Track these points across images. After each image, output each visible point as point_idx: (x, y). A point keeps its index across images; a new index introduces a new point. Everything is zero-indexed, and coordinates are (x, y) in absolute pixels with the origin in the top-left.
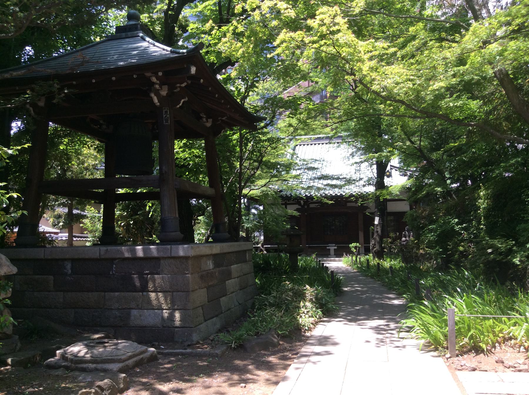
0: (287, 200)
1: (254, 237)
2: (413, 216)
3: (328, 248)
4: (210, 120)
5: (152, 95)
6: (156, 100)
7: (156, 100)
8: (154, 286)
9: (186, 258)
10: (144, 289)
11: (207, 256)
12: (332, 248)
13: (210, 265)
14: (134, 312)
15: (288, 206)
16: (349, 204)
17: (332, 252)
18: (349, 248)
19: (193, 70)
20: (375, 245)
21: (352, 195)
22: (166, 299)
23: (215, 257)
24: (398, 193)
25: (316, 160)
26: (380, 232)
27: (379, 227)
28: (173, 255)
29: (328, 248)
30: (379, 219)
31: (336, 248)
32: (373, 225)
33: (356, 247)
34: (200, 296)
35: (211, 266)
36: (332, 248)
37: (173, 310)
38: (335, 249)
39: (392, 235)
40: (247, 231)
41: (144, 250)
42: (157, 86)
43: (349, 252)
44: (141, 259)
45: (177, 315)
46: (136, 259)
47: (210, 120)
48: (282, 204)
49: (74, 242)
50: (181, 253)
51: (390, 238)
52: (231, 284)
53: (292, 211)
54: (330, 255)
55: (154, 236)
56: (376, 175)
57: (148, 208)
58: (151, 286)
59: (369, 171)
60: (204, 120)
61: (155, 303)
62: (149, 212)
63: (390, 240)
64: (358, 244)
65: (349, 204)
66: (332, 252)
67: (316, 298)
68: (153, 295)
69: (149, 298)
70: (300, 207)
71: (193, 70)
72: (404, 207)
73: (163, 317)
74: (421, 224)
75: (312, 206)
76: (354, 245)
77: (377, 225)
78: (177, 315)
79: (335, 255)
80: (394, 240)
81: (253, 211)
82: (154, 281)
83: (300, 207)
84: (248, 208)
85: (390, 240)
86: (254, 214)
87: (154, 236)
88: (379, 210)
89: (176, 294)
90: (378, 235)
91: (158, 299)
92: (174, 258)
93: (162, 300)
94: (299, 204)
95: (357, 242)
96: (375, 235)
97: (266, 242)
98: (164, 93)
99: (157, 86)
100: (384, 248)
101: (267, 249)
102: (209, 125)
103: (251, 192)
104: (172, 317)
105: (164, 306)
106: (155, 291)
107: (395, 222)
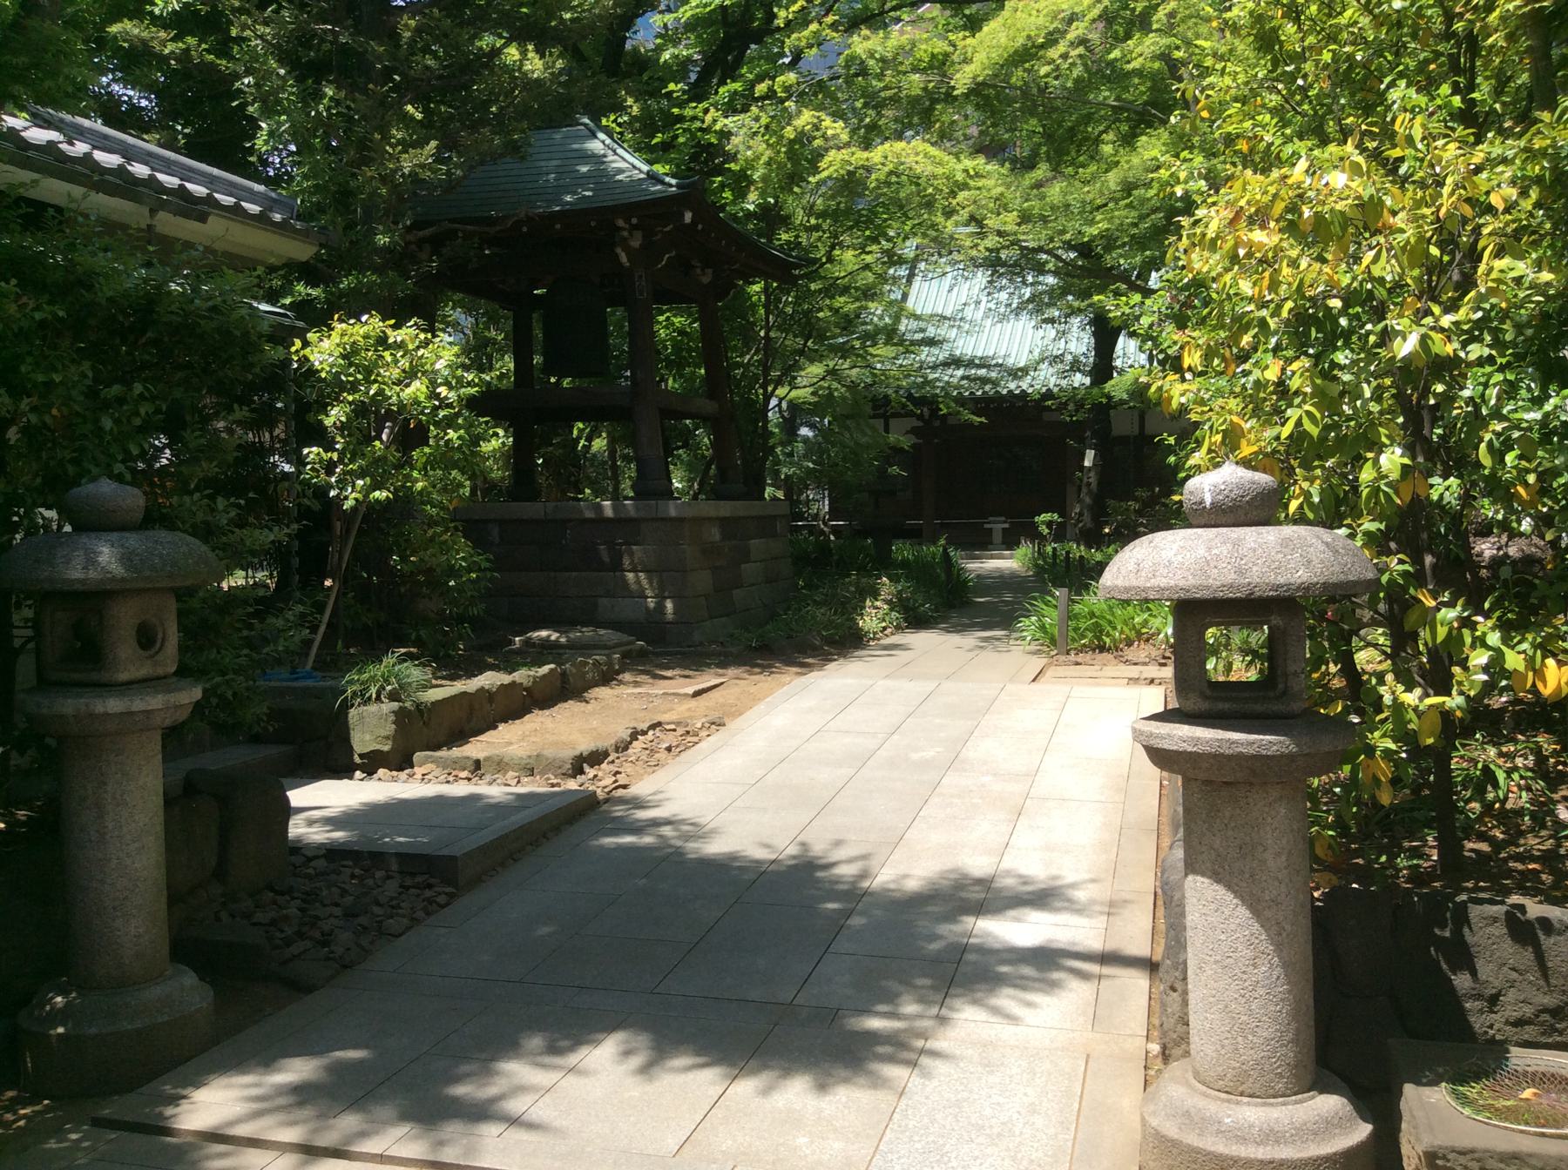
0: (877, 405)
1: (808, 500)
4: (710, 271)
5: (619, 250)
6: (624, 258)
7: (624, 258)
8: (632, 562)
9: (680, 520)
10: (617, 567)
11: (710, 519)
12: (998, 526)
13: (715, 534)
14: (604, 601)
15: (893, 422)
17: (997, 537)
18: (1035, 526)
19: (688, 217)
20: (1081, 514)
22: (651, 583)
23: (723, 522)
24: (1125, 396)
25: (945, 318)
26: (1094, 486)
27: (1092, 474)
28: (660, 515)
32: (1082, 468)
33: (1049, 524)
34: (702, 580)
35: (717, 537)
37: (661, 598)
40: (789, 485)
41: (614, 508)
42: (625, 234)
43: (1033, 534)
44: (609, 520)
45: (669, 605)
46: (601, 521)
47: (710, 271)
48: (874, 417)
50: (673, 513)
51: (1136, 499)
52: (750, 570)
53: (900, 437)
55: (588, 491)
57: (575, 432)
58: (626, 562)
59: (1080, 342)
60: (699, 271)
61: (634, 587)
62: (579, 438)
66: (997, 537)
67: (900, 599)
68: (630, 575)
69: (625, 581)
70: (920, 424)
71: (688, 217)
73: (647, 608)
77: (1090, 469)
78: (669, 605)
81: (804, 431)
82: (631, 554)
83: (920, 424)
84: (790, 427)
86: (806, 440)
87: (588, 491)
89: (667, 574)
90: (1090, 492)
91: (638, 582)
92: (662, 519)
93: (645, 583)
96: (1084, 490)
97: (835, 513)
98: (636, 243)
99: (625, 234)
101: (835, 530)
102: (706, 280)
103: (794, 394)
104: (660, 607)
105: (649, 593)
106: (634, 570)
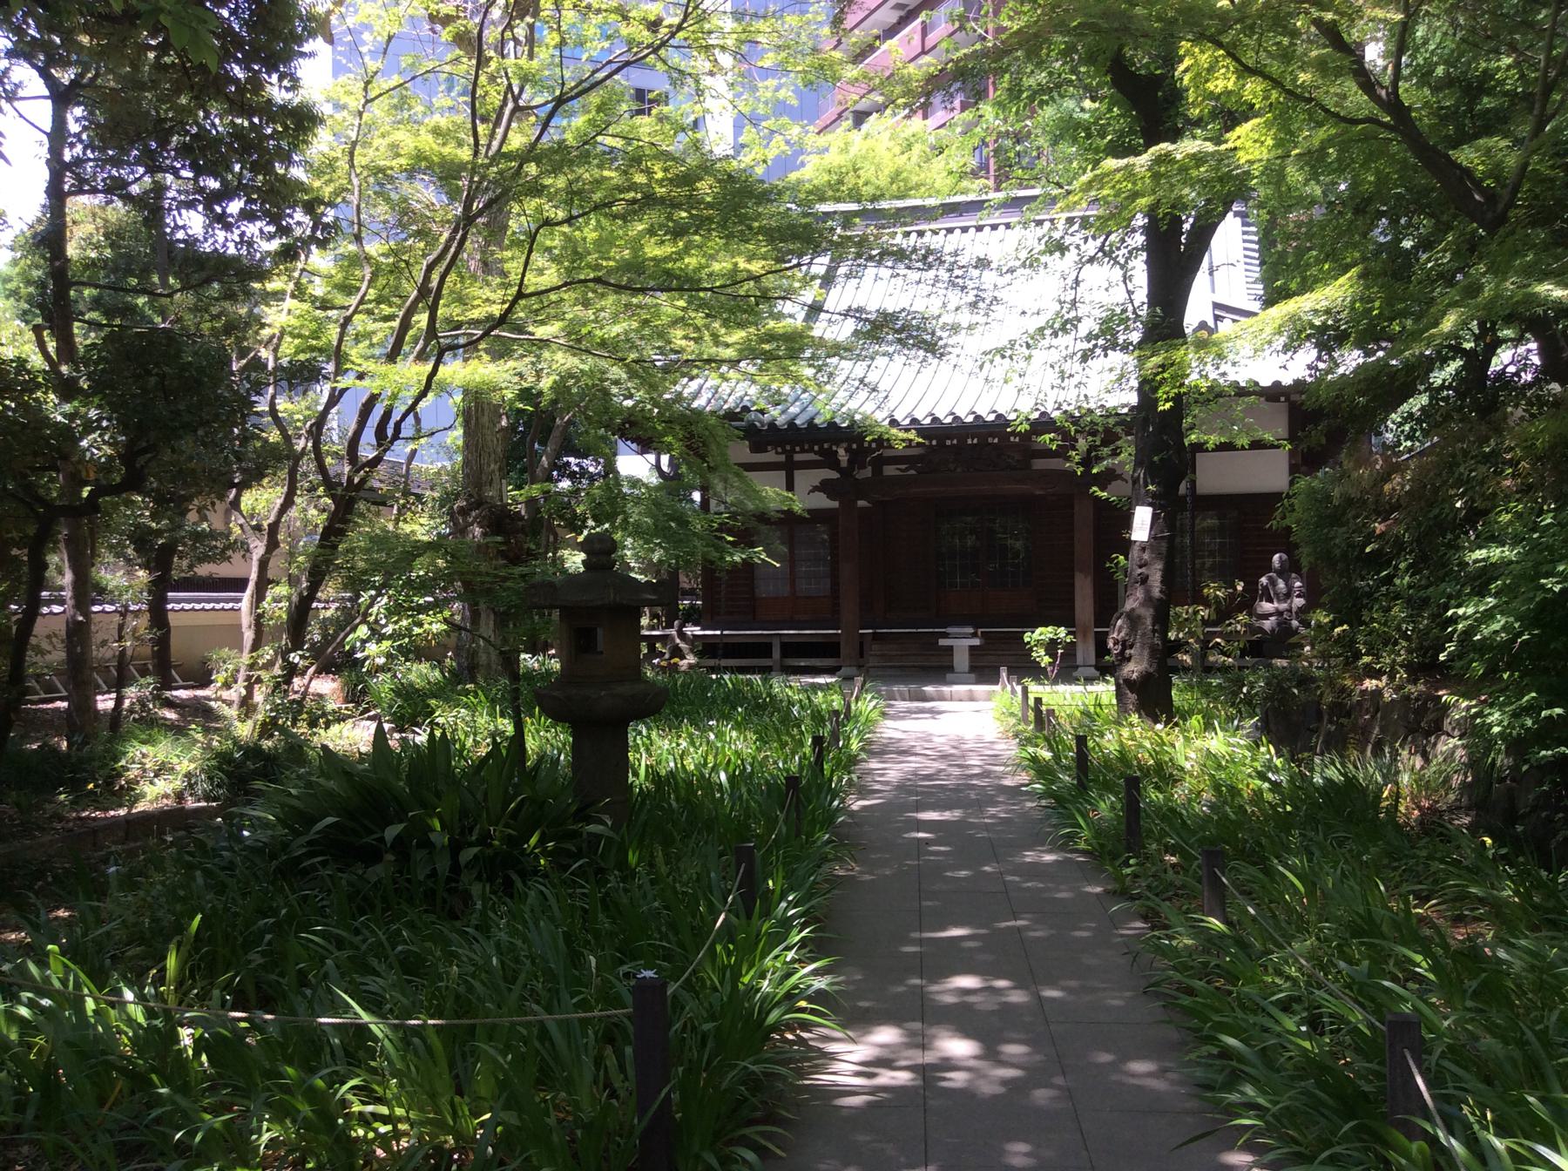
2: (1328, 498)
3: (942, 642)
12: (962, 642)
16: (1039, 464)
17: (961, 660)
18: (1026, 651)
21: (1044, 424)
29: (942, 642)
30: (1155, 517)
31: (976, 642)
32: (1126, 546)
33: (1051, 647)
36: (962, 642)
38: (972, 648)
39: (1215, 591)
43: (1025, 668)
49: (171, 616)
51: (1206, 603)
54: (951, 669)
56: (1141, 296)
63: (1204, 613)
64: (1062, 632)
65: (1039, 464)
66: (961, 660)
70: (834, 475)
72: (1268, 473)
74: (1370, 537)
75: (890, 470)
76: (1044, 633)
79: (973, 669)
80: (1224, 612)
85: (1204, 613)
88: (1153, 472)
94: (830, 460)
95: (1067, 620)
100: (1178, 646)
107: (1225, 538)
